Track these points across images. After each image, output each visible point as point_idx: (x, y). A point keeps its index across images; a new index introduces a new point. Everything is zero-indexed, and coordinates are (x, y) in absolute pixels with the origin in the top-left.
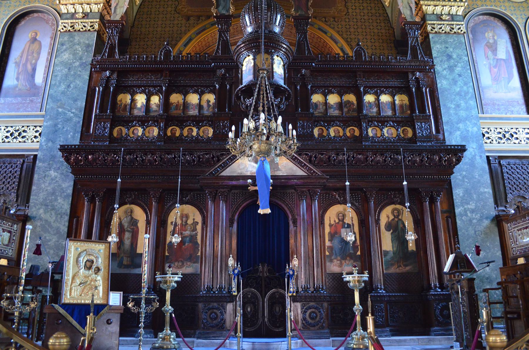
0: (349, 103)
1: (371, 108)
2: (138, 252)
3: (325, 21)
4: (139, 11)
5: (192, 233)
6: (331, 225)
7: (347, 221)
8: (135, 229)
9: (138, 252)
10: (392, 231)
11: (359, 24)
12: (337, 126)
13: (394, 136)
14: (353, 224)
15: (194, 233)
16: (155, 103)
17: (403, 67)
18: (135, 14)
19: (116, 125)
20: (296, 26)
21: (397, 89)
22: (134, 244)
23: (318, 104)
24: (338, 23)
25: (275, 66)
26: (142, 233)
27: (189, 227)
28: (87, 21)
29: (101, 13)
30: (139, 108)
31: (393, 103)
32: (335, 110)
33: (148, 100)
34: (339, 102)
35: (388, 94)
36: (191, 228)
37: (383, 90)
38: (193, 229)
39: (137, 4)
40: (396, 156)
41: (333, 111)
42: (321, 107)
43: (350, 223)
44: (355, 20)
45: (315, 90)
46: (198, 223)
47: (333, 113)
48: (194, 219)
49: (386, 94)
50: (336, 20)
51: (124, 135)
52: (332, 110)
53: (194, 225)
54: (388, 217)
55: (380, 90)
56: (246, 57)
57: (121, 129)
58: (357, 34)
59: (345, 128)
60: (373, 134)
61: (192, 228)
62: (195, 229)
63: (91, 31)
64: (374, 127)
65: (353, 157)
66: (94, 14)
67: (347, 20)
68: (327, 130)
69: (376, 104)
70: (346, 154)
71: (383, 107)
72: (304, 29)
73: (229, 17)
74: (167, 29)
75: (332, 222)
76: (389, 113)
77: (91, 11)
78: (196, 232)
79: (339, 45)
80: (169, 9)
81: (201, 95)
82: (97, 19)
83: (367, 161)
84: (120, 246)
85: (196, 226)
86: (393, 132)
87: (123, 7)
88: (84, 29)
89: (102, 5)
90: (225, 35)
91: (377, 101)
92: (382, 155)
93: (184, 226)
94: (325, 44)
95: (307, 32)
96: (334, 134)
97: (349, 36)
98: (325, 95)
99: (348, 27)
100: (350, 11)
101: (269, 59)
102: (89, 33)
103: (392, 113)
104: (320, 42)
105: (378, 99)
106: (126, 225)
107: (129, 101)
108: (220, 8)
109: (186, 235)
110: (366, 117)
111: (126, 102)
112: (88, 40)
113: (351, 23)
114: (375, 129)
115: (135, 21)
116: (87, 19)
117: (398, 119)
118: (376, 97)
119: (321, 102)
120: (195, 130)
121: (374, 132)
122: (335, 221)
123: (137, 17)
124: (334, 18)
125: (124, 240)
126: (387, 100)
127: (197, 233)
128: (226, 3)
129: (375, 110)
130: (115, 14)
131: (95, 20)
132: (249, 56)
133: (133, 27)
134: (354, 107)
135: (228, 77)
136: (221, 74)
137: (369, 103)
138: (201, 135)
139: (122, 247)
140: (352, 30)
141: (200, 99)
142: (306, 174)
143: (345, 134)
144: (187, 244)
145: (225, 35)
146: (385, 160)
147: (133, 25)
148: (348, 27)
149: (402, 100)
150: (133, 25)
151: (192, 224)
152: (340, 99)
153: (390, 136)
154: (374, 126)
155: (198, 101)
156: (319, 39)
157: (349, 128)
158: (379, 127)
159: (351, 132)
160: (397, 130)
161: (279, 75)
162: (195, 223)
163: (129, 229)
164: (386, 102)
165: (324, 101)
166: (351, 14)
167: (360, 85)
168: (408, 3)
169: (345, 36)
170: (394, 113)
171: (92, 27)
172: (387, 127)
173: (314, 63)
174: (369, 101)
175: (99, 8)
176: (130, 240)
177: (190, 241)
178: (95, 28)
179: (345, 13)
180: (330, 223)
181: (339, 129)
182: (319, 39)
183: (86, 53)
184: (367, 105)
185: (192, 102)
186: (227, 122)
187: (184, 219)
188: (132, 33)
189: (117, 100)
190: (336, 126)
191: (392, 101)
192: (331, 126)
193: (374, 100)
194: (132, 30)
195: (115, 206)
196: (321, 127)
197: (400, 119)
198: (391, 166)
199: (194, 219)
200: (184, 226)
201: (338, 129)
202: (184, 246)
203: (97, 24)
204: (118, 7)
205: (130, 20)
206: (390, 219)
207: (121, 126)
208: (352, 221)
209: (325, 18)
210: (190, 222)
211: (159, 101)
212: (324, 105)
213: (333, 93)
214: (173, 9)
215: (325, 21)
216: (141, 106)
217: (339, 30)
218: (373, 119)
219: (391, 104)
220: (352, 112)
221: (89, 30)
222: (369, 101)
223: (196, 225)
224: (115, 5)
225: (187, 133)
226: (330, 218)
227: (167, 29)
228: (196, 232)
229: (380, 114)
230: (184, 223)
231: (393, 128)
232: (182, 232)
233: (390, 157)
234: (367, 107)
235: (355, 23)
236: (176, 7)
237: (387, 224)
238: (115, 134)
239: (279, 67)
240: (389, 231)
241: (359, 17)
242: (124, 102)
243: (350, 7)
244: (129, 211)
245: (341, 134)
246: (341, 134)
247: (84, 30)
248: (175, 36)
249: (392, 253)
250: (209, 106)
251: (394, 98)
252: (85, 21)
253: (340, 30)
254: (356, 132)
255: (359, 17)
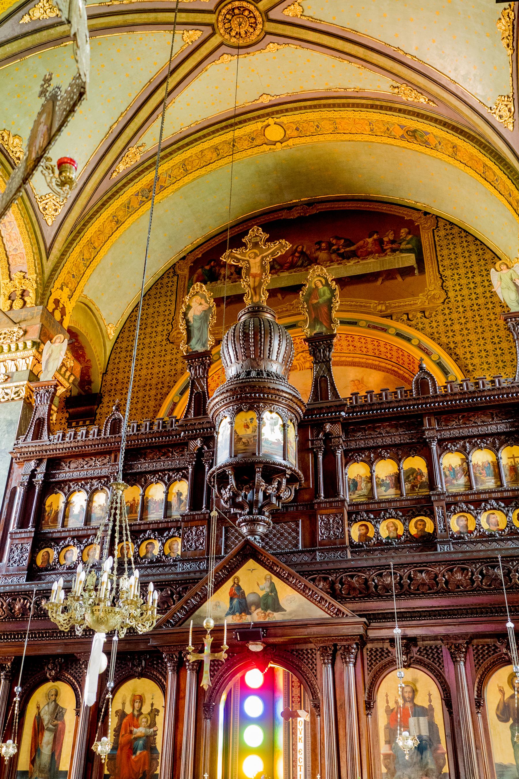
0: (413, 474)
1: (455, 477)
2: (60, 769)
3: (408, 319)
4: (115, 347)
5: (148, 730)
6: (389, 712)
7: (421, 700)
8: (60, 726)
9: (60, 769)
10: (511, 721)
11: (469, 314)
12: (393, 517)
13: (502, 526)
14: (431, 706)
15: (152, 730)
16: (100, 505)
17: (508, 396)
18: (108, 354)
19: (41, 546)
20: (313, 353)
21: (503, 437)
22: (57, 754)
23: (358, 480)
24: (431, 319)
25: (264, 430)
26: (69, 732)
27: (144, 720)
28: (11, 385)
29: (31, 371)
30: (76, 515)
31: (496, 465)
32: (388, 487)
33: (90, 501)
34: (396, 474)
35: (485, 448)
36: (147, 722)
37: (476, 442)
38: (150, 725)
39: (111, 338)
40: (491, 571)
41: (385, 491)
42: (363, 485)
43: (426, 705)
44: (461, 309)
45: (352, 456)
46: (158, 711)
47: (385, 493)
48: (152, 705)
49: (481, 448)
50: (427, 314)
51: (51, 561)
52: (383, 488)
53: (152, 715)
54: (502, 691)
55: (470, 443)
56: (222, 420)
57: (47, 552)
58: (465, 332)
59: (405, 520)
60: (461, 527)
61: (149, 722)
62: (153, 724)
63: (16, 400)
64: (462, 514)
65: (409, 577)
66: (21, 373)
67: (447, 311)
68: (375, 526)
69: (463, 470)
70: (395, 573)
71: (478, 475)
72: (325, 356)
73: (206, 354)
74: (156, 370)
75: (392, 705)
76: (490, 483)
77: (17, 370)
78: (155, 729)
79: (435, 357)
80: (159, 338)
81: (168, 486)
82: (24, 380)
83: (437, 583)
84: (34, 758)
85: (155, 717)
86: (498, 519)
87: (58, 359)
88: (6, 397)
89: (31, 358)
90: (200, 384)
91: (465, 464)
92: (463, 570)
93: (135, 718)
94: (411, 358)
95: (330, 360)
96: (387, 532)
97: (451, 339)
98: (371, 464)
99: (449, 323)
100: (451, 294)
101: (255, 419)
102: (13, 403)
103: (496, 483)
104: (403, 355)
105: (466, 461)
106: (46, 718)
107: (62, 506)
108: (193, 341)
109: (139, 734)
110: (442, 497)
111: (58, 507)
112: (11, 413)
113: (455, 316)
114: (464, 516)
115: (108, 363)
116: (11, 382)
117: (505, 494)
118: (464, 457)
119: (364, 477)
120: (157, 544)
121: (463, 522)
122: (397, 702)
123: (113, 357)
124: (424, 312)
125: (42, 747)
126: (485, 460)
127: (155, 731)
128: (202, 333)
129: (462, 480)
130: (46, 371)
131: (22, 383)
132: (226, 417)
133: (105, 374)
134: (424, 479)
135: (207, 452)
136: (196, 448)
137: (451, 469)
138: (166, 554)
139: (37, 759)
140: (456, 327)
141: (167, 493)
142: (328, 616)
143: (407, 531)
144: (138, 752)
145: (200, 384)
146: (471, 579)
147: (106, 371)
148: (449, 323)
149: (514, 457)
150: (106, 371)
151: (149, 714)
152: (397, 467)
153: (494, 528)
154: (461, 512)
155: (163, 496)
156: (399, 351)
157: (414, 521)
158: (470, 513)
159: (418, 526)
160: (507, 515)
161: (273, 443)
162: (154, 712)
163: (51, 726)
164: (483, 463)
165: (369, 475)
166: (452, 300)
167: (429, 438)
168: (512, 280)
169: (444, 340)
170: (499, 483)
171: (17, 395)
172: (486, 511)
173: (343, 411)
174: (450, 465)
175: (27, 364)
176: (50, 746)
177: (145, 747)
178: (21, 395)
179: (442, 301)
180: (388, 707)
181: (398, 522)
182: (399, 351)
183: (6, 435)
184: (447, 473)
185: (154, 498)
186: (203, 529)
187: (137, 705)
188: (104, 383)
189: (45, 505)
190: (389, 518)
191: (495, 460)
192: (381, 518)
193: (460, 462)
194: (104, 378)
195: (15, 690)
196: (363, 523)
197: (510, 494)
198: (486, 590)
199: (152, 705)
200: (135, 718)
201: (394, 524)
202: (133, 757)
203: (24, 389)
204: (51, 360)
205: (100, 364)
206: (507, 696)
207: (48, 547)
208: (430, 701)
209: (407, 314)
210: (146, 709)
211: (106, 501)
212: (368, 482)
213: (383, 458)
214: (165, 337)
215: (408, 319)
216: (80, 512)
217: (433, 330)
218: (458, 498)
219: (494, 466)
220: (420, 488)
221: (13, 399)
222: (450, 465)
223: (155, 715)
224: (47, 357)
225: (145, 551)
226: (387, 696)
227: (156, 370)
228: (155, 729)
229: (471, 488)
230: (136, 713)
231: (499, 512)
232: (132, 728)
233: (481, 573)
234: (446, 476)
235: (462, 315)
236: (169, 334)
237: (501, 707)
238: (39, 561)
239: (273, 430)
240: (507, 721)
241: (468, 303)
242: (54, 507)
243: (450, 289)
244: (53, 692)
245: (400, 532)
246: (400, 532)
247: (6, 399)
248: (168, 379)
249: (514, 769)
250: (180, 501)
251: (497, 456)
252: (8, 385)
253: (435, 330)
254: (427, 525)
255: (468, 303)
